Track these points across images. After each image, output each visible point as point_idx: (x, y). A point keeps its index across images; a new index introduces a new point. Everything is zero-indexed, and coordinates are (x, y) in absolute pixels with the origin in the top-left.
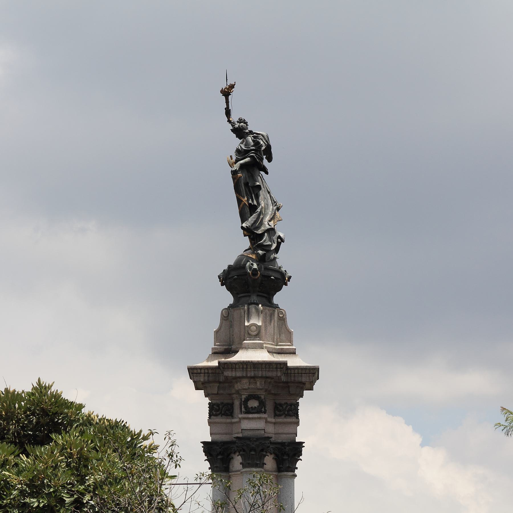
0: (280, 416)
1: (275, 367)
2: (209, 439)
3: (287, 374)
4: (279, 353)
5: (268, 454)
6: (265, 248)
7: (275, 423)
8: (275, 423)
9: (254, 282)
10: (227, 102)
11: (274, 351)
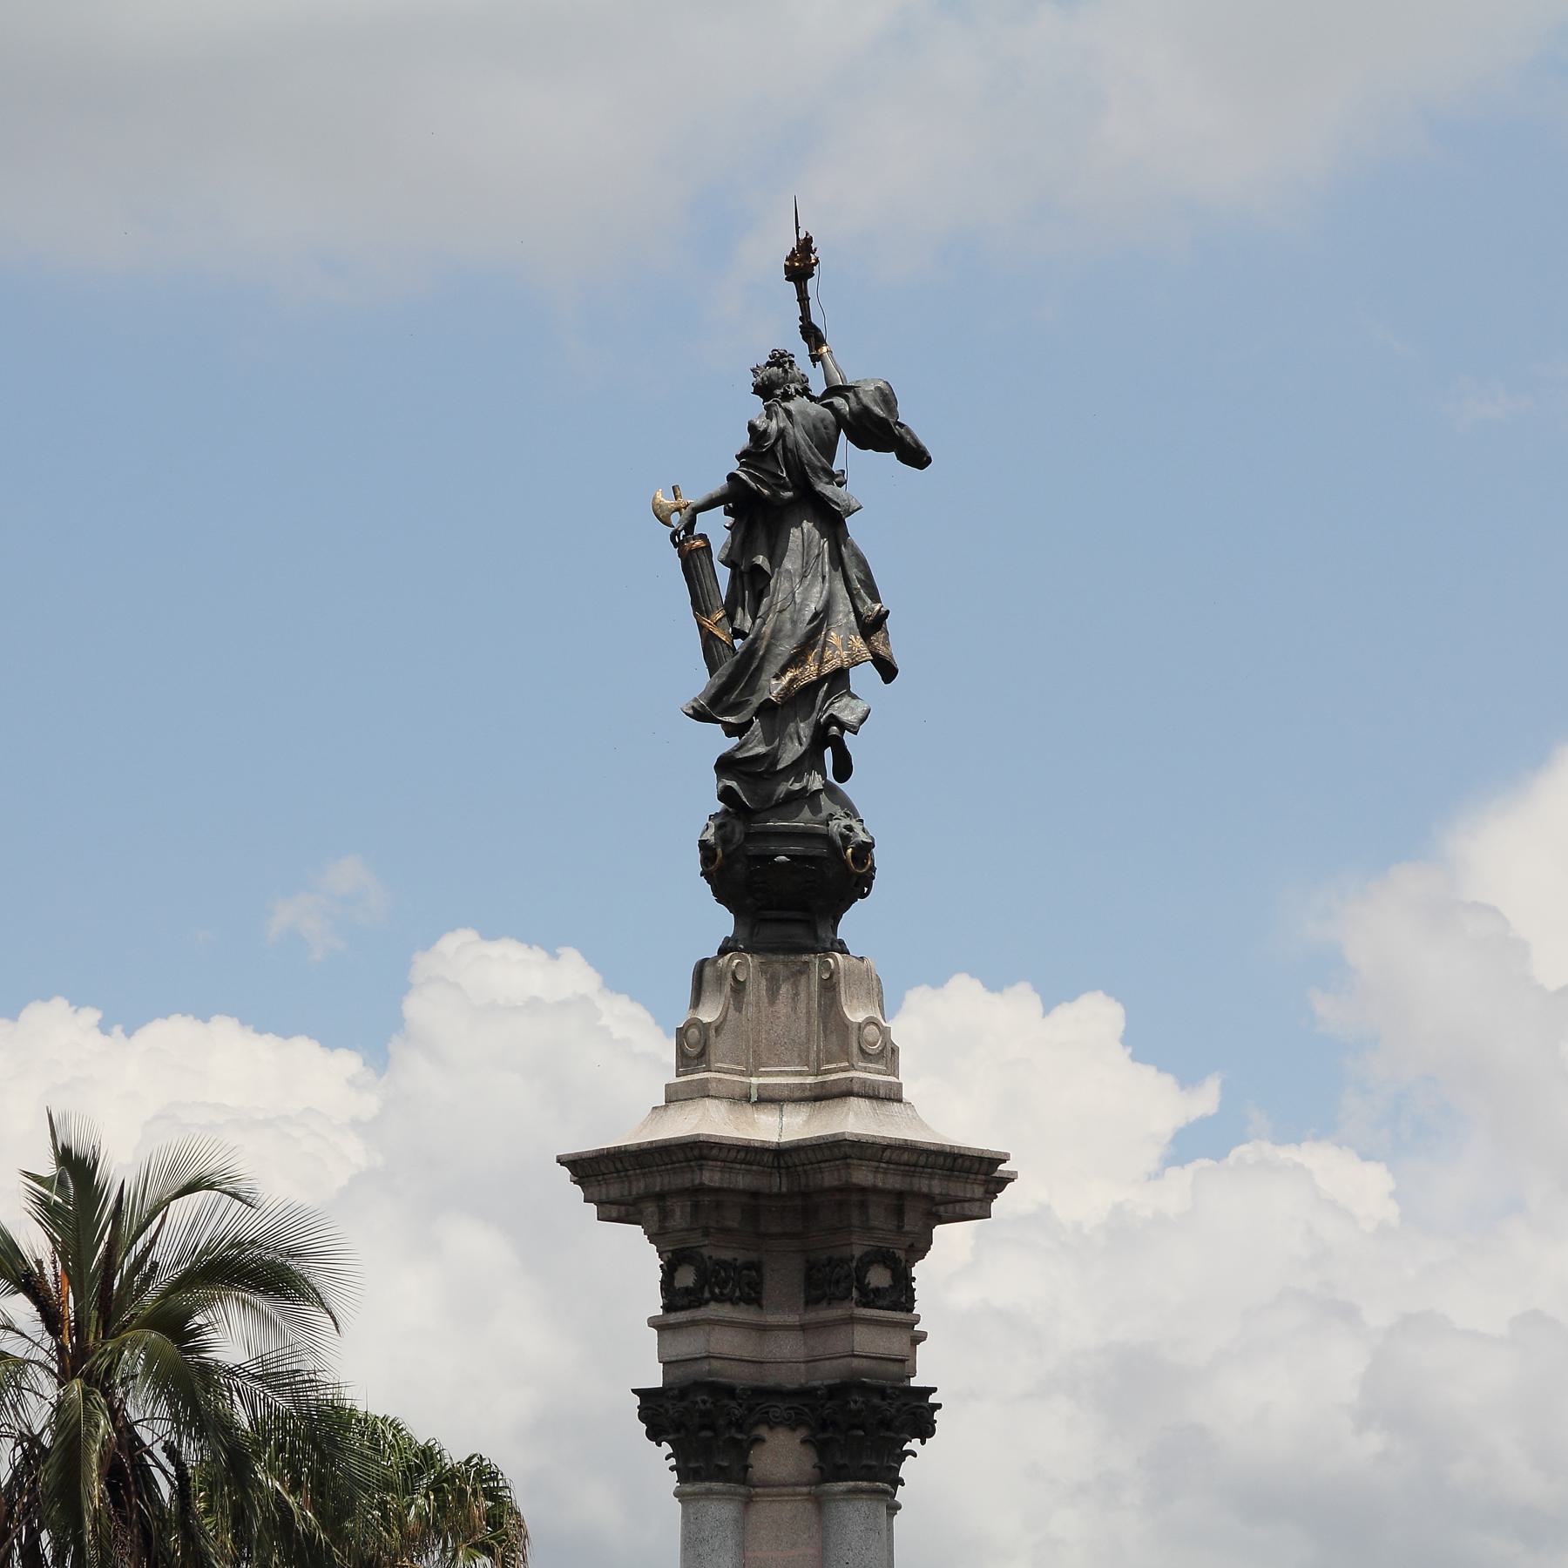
0: (832, 1300)
1: (681, 1156)
2: (655, 1379)
3: (779, 1167)
4: (817, 1099)
5: (763, 1431)
6: (743, 769)
7: (803, 1328)
8: (803, 1328)
9: (785, 878)
10: (803, 299)
11: (797, 1094)
